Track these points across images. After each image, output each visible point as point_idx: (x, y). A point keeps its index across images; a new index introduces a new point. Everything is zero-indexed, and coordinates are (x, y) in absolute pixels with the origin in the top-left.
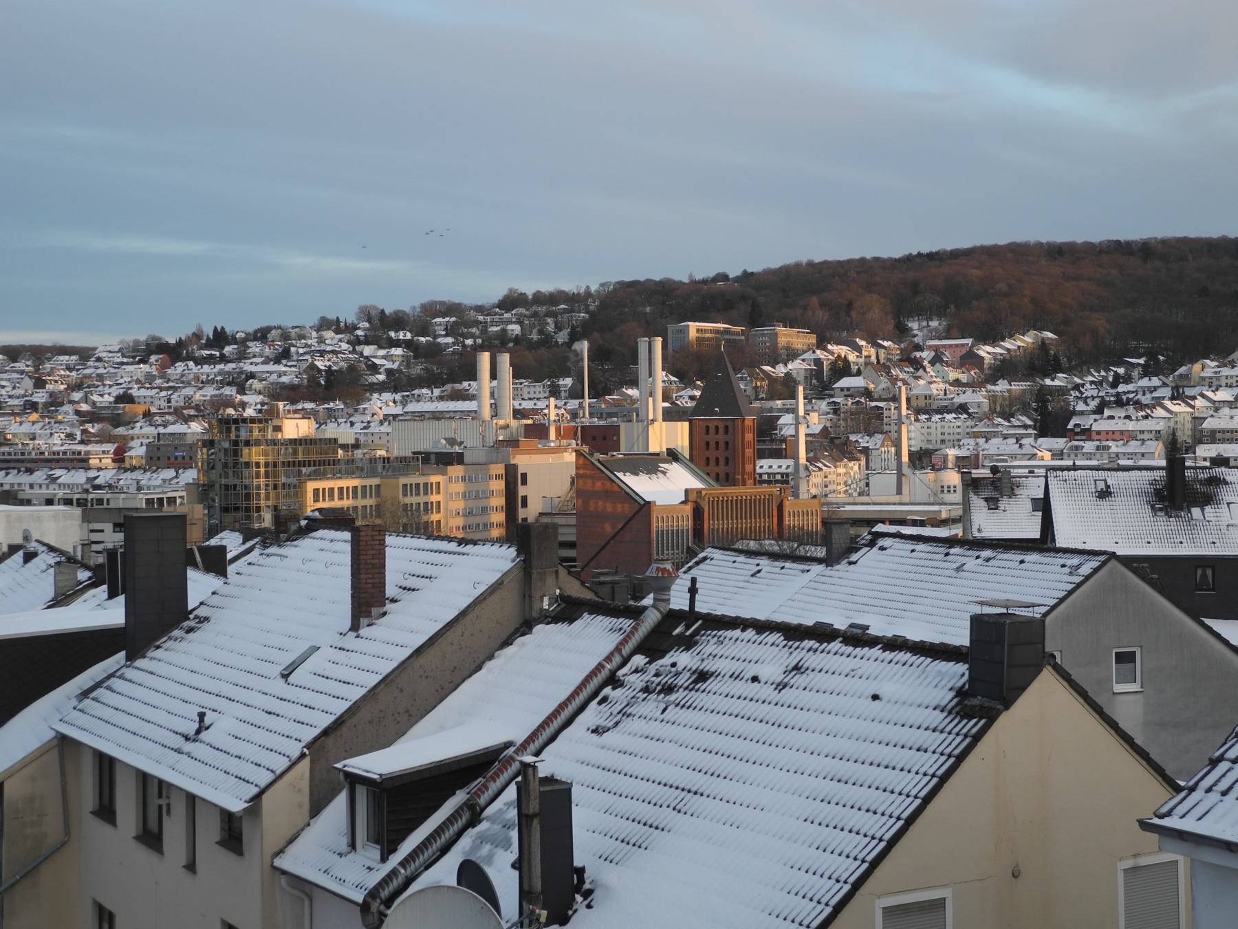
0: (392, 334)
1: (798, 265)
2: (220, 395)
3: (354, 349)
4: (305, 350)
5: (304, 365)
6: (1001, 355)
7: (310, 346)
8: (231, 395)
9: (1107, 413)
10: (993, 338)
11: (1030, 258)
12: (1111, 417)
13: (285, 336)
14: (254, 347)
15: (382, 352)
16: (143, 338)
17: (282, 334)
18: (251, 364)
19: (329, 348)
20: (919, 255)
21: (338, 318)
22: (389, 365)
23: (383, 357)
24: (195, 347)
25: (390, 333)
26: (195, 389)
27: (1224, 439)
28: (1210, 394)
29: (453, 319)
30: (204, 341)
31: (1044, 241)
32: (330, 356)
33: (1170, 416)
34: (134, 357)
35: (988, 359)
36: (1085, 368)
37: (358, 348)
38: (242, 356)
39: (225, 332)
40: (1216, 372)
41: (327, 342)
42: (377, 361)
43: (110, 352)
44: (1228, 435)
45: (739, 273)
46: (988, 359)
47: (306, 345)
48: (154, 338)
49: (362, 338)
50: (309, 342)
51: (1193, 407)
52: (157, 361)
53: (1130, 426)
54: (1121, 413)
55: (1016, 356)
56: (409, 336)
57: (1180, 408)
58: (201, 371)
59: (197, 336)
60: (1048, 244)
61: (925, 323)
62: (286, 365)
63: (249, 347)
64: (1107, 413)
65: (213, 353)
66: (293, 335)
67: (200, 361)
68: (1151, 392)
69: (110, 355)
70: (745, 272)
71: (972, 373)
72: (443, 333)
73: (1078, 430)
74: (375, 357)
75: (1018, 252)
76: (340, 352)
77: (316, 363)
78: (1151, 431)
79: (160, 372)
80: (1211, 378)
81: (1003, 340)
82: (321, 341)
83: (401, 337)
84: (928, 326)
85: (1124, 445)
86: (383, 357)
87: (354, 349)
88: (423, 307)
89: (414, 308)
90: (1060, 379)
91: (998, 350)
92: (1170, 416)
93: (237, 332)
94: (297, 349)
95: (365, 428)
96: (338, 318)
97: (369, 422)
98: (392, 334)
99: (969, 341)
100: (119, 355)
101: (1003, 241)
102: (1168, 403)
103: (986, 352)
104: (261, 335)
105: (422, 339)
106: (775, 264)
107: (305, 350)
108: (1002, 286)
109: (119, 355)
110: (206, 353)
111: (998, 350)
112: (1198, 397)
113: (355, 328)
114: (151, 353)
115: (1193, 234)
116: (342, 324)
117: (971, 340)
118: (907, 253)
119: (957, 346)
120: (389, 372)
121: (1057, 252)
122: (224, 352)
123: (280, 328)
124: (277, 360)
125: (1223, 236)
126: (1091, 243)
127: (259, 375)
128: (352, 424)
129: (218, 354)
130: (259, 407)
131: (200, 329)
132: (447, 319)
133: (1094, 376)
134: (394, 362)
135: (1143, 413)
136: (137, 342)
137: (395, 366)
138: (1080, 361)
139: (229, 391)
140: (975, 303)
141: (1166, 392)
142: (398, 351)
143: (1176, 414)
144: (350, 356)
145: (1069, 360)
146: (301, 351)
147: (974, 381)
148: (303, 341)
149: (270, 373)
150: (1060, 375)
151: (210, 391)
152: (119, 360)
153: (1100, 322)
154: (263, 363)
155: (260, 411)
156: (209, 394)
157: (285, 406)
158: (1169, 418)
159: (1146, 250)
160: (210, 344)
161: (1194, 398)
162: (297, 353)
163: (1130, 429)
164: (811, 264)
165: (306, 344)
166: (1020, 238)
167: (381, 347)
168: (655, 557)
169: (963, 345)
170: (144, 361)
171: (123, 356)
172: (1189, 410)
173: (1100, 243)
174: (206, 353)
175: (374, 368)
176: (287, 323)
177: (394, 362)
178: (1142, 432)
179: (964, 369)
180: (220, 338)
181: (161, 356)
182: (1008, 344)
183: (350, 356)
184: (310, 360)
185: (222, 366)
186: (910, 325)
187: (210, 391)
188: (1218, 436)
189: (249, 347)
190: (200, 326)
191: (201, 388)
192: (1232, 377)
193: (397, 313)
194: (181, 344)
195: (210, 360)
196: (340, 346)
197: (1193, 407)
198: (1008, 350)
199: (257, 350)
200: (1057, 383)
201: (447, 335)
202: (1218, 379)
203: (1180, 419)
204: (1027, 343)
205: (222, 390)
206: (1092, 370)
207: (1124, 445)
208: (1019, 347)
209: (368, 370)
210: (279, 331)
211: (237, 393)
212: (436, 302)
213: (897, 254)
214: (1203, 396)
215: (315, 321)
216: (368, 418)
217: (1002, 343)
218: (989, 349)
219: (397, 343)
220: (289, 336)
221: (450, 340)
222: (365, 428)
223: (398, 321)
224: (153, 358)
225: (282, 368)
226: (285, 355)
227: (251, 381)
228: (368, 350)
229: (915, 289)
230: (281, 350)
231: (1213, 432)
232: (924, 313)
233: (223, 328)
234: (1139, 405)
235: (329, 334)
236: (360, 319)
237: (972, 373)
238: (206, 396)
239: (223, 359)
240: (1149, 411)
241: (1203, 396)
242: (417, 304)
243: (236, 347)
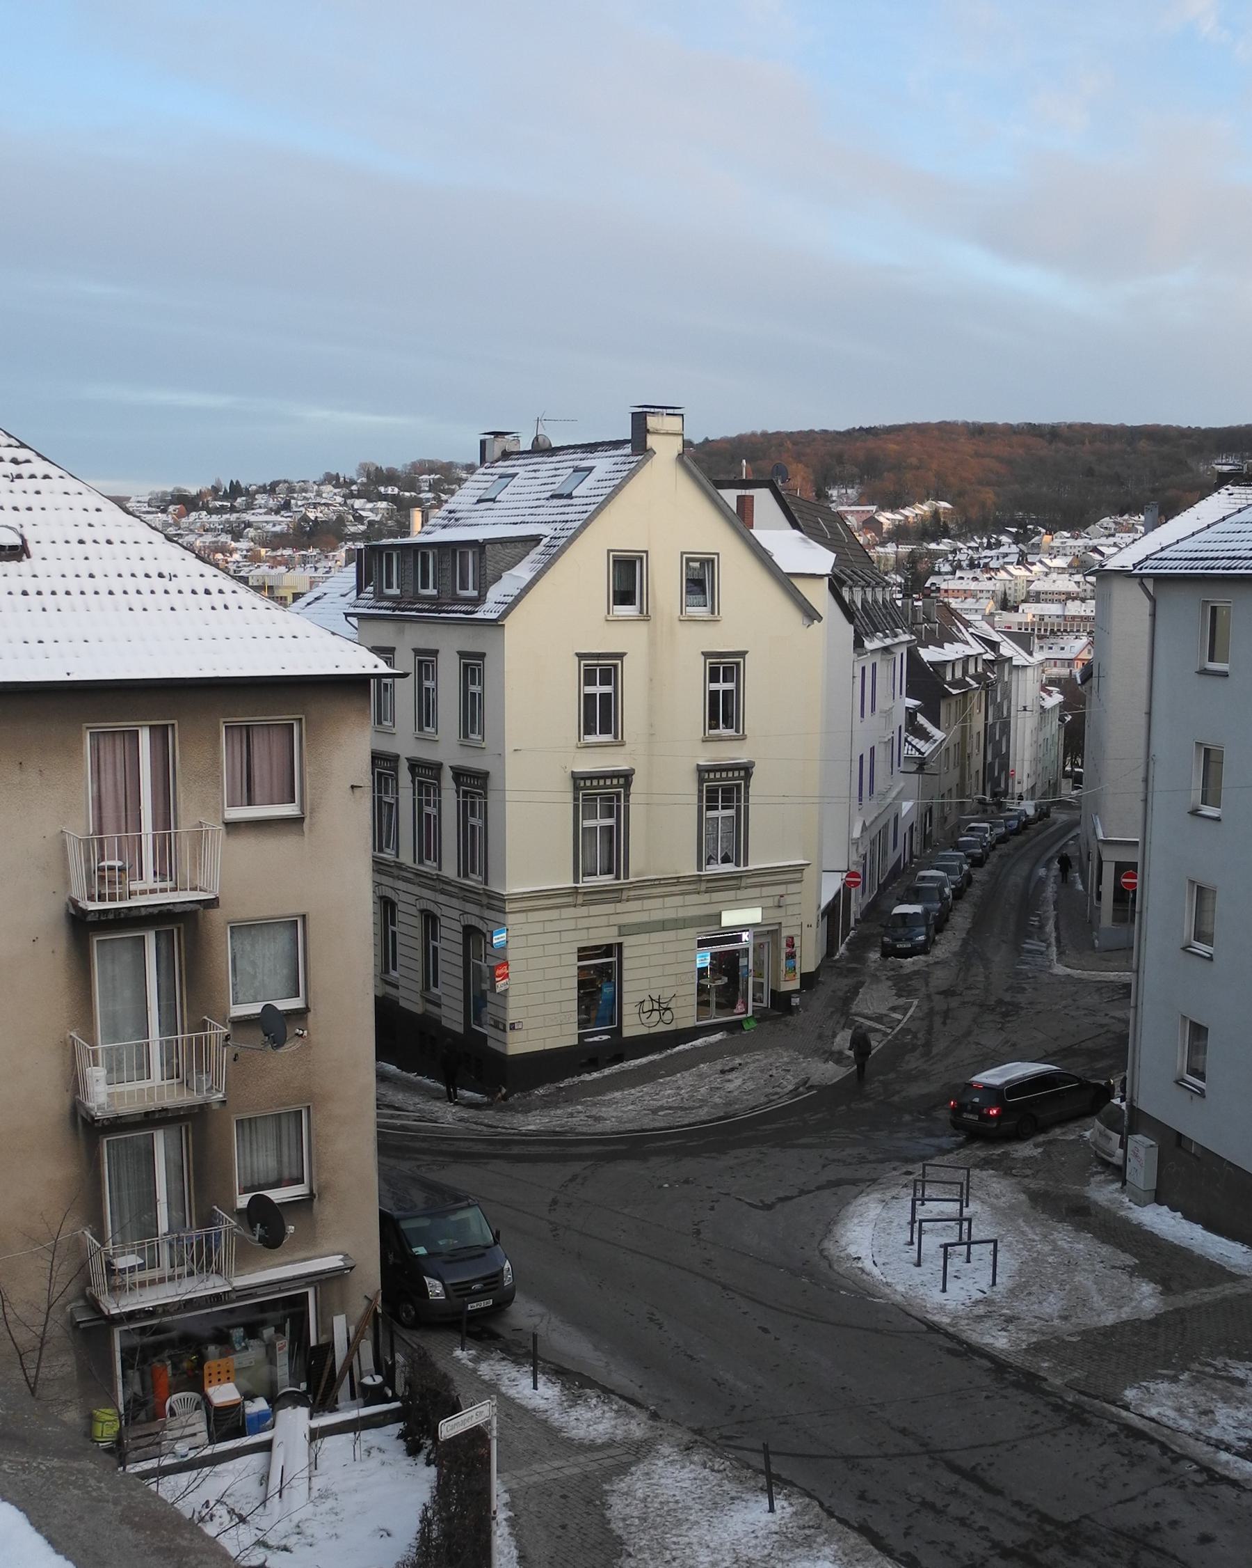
0: (382, 489)
1: (754, 435)
2: (217, 542)
3: (345, 502)
4: (303, 502)
5: (298, 516)
6: (900, 521)
7: (308, 499)
8: (226, 543)
9: (959, 574)
10: (894, 504)
11: (953, 436)
12: (961, 578)
13: (291, 490)
14: (261, 499)
15: (370, 505)
16: (170, 489)
17: (288, 488)
18: (253, 514)
19: (323, 501)
20: (861, 429)
21: (338, 474)
22: (372, 517)
23: (371, 510)
24: (210, 498)
25: (380, 488)
26: (196, 536)
27: (1046, 600)
28: (1047, 561)
29: (438, 476)
30: (221, 493)
31: (970, 421)
32: (322, 508)
33: (1011, 578)
34: (158, 507)
35: (887, 525)
36: (969, 535)
37: (349, 501)
38: (249, 507)
39: (240, 485)
40: (1062, 543)
41: (324, 495)
42: (363, 513)
43: (139, 502)
44: (1050, 597)
45: (701, 440)
46: (887, 525)
47: (305, 498)
48: (179, 490)
49: (356, 492)
50: (308, 495)
51: (1031, 571)
52: (174, 511)
53: (973, 586)
54: (968, 574)
55: (915, 522)
56: (396, 490)
57: (1020, 572)
58: (210, 520)
59: (215, 490)
60: (973, 424)
61: (844, 491)
62: (282, 516)
63: (256, 499)
64: (959, 574)
65: (225, 504)
66: (297, 488)
67: (211, 512)
68: (1004, 557)
69: (138, 505)
70: (707, 439)
71: (869, 536)
72: (427, 489)
73: (933, 588)
74: (363, 510)
75: (945, 430)
76: (331, 505)
77: (309, 514)
78: (989, 591)
79: (175, 521)
80: (1058, 547)
81: (903, 508)
82: (319, 494)
83: (389, 492)
84: (846, 493)
85: (962, 602)
86: (371, 510)
87: (345, 502)
88: (413, 464)
89: (405, 466)
90: (944, 544)
91: (898, 517)
92: (1011, 578)
93: (250, 485)
94: (297, 502)
95: (327, 572)
96: (338, 474)
97: (330, 568)
98: (382, 489)
99: (874, 508)
100: (146, 505)
101: (935, 419)
102: (1010, 568)
103: (887, 519)
104: (271, 489)
105: (407, 494)
106: (733, 433)
107: (303, 502)
108: (914, 461)
109: (146, 505)
110: (218, 504)
111: (898, 517)
112: (1038, 563)
113: (353, 482)
114: (172, 503)
115: (1095, 421)
116: (342, 479)
117: (875, 507)
118: (851, 427)
119: (863, 511)
120: (371, 523)
121: (980, 432)
122: (235, 504)
123: (285, 482)
124: (277, 512)
125: (1122, 424)
126: (1011, 425)
127: (255, 524)
128: (316, 569)
129: (229, 504)
130: (245, 553)
131: (218, 481)
132: (432, 476)
133: (976, 542)
134: (377, 514)
135: (989, 576)
136: (165, 493)
137: (377, 518)
138: (967, 528)
139: (226, 538)
140: (885, 474)
141: (1014, 558)
142: (383, 505)
143: (1016, 577)
144: (341, 508)
145: (960, 527)
146: (300, 503)
147: (869, 544)
148: (304, 494)
149: (267, 522)
150: (946, 540)
151: (209, 538)
152: (144, 509)
153: (989, 495)
154: (265, 513)
155: (245, 557)
156: (208, 541)
157: (266, 552)
158: (1010, 581)
159: (1053, 433)
160: (226, 497)
161: (1033, 564)
162: (296, 505)
163: (972, 588)
164: (765, 435)
165: (305, 497)
166: (949, 418)
167: (370, 501)
168: (583, 662)
169: (868, 511)
170: (164, 511)
171: (149, 506)
172: (1028, 573)
173: (1018, 425)
174: (218, 504)
175: (359, 519)
176: (294, 478)
177: (377, 514)
178: (982, 591)
179: (861, 532)
180: (235, 490)
181: (178, 507)
182: (908, 512)
183: (341, 508)
184: (304, 511)
185: (228, 516)
186: (830, 492)
187: (209, 538)
188: (1042, 596)
189: (256, 499)
190: (219, 479)
191: (201, 535)
192: (1075, 547)
193: (389, 470)
194: (200, 495)
195: (220, 511)
196: (335, 500)
197: (1031, 571)
198: (907, 517)
199: (263, 502)
200: (942, 547)
201: (429, 491)
202: (1064, 548)
203: (1019, 581)
204: (925, 512)
205: (219, 538)
206: (975, 537)
207: (962, 602)
208: (917, 515)
209: (355, 521)
210: (286, 485)
211: (232, 540)
212: (425, 460)
213: (842, 428)
214: (1041, 562)
215: (319, 476)
216: (330, 564)
217: (902, 511)
218: (889, 515)
219: (384, 498)
220: (294, 490)
221: (430, 495)
222: (327, 572)
223: (389, 477)
224: (171, 508)
225: (278, 518)
226: (286, 506)
227: (248, 529)
228: (358, 503)
229: (840, 459)
230: (282, 502)
231: (1038, 593)
232: (846, 482)
233: (237, 482)
234: (986, 568)
235: (328, 489)
236: (359, 475)
237: (869, 536)
238: (205, 542)
239: (233, 509)
240: (993, 574)
241: (1041, 562)
242: (409, 462)
243: (244, 498)
